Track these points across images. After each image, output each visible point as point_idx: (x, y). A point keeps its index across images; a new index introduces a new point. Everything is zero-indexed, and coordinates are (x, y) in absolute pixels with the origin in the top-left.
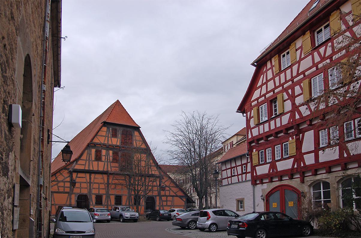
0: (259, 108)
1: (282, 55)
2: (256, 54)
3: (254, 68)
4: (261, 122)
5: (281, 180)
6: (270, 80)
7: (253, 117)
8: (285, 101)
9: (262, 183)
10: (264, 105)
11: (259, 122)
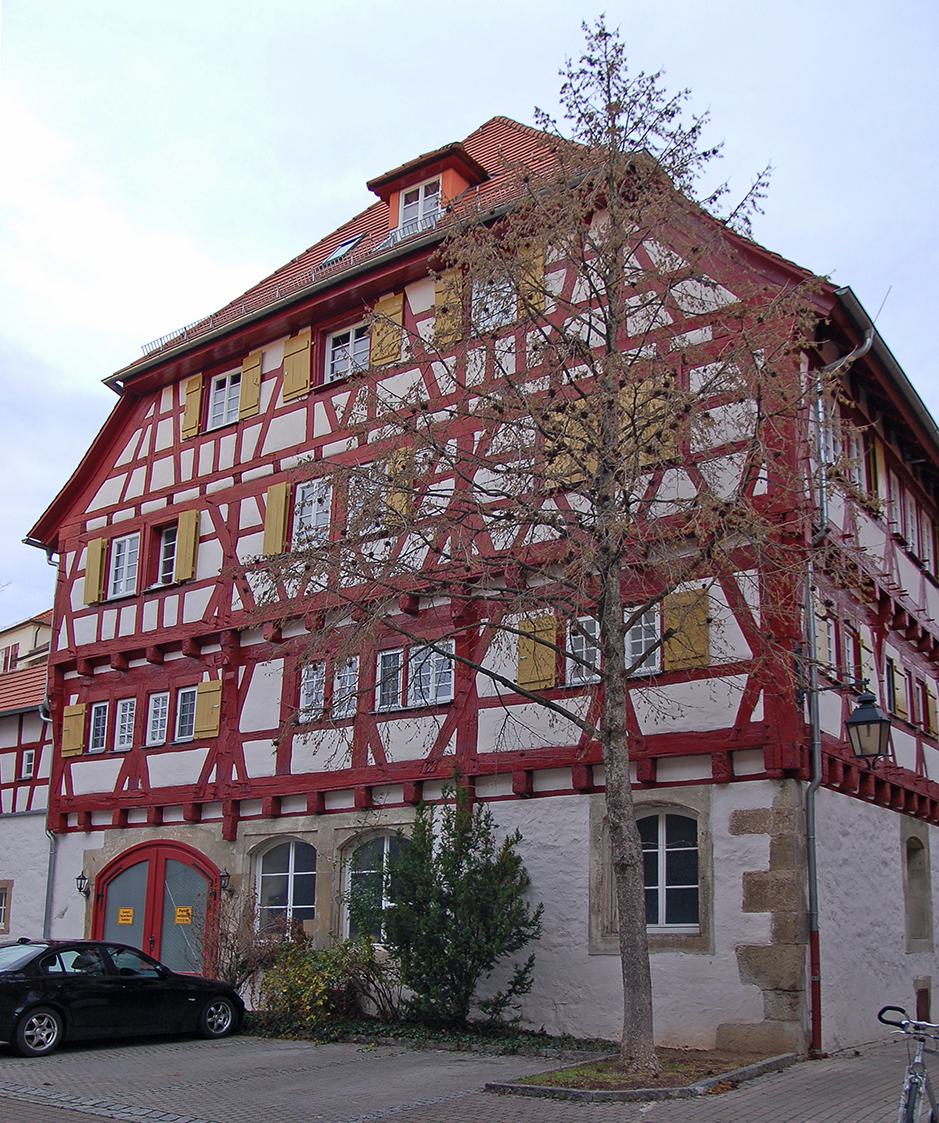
0: (110, 543)
1: (215, 380)
2: (128, 354)
3: (114, 398)
4: (111, 596)
6: (165, 454)
7: (83, 573)
8: (203, 539)
10: (131, 540)
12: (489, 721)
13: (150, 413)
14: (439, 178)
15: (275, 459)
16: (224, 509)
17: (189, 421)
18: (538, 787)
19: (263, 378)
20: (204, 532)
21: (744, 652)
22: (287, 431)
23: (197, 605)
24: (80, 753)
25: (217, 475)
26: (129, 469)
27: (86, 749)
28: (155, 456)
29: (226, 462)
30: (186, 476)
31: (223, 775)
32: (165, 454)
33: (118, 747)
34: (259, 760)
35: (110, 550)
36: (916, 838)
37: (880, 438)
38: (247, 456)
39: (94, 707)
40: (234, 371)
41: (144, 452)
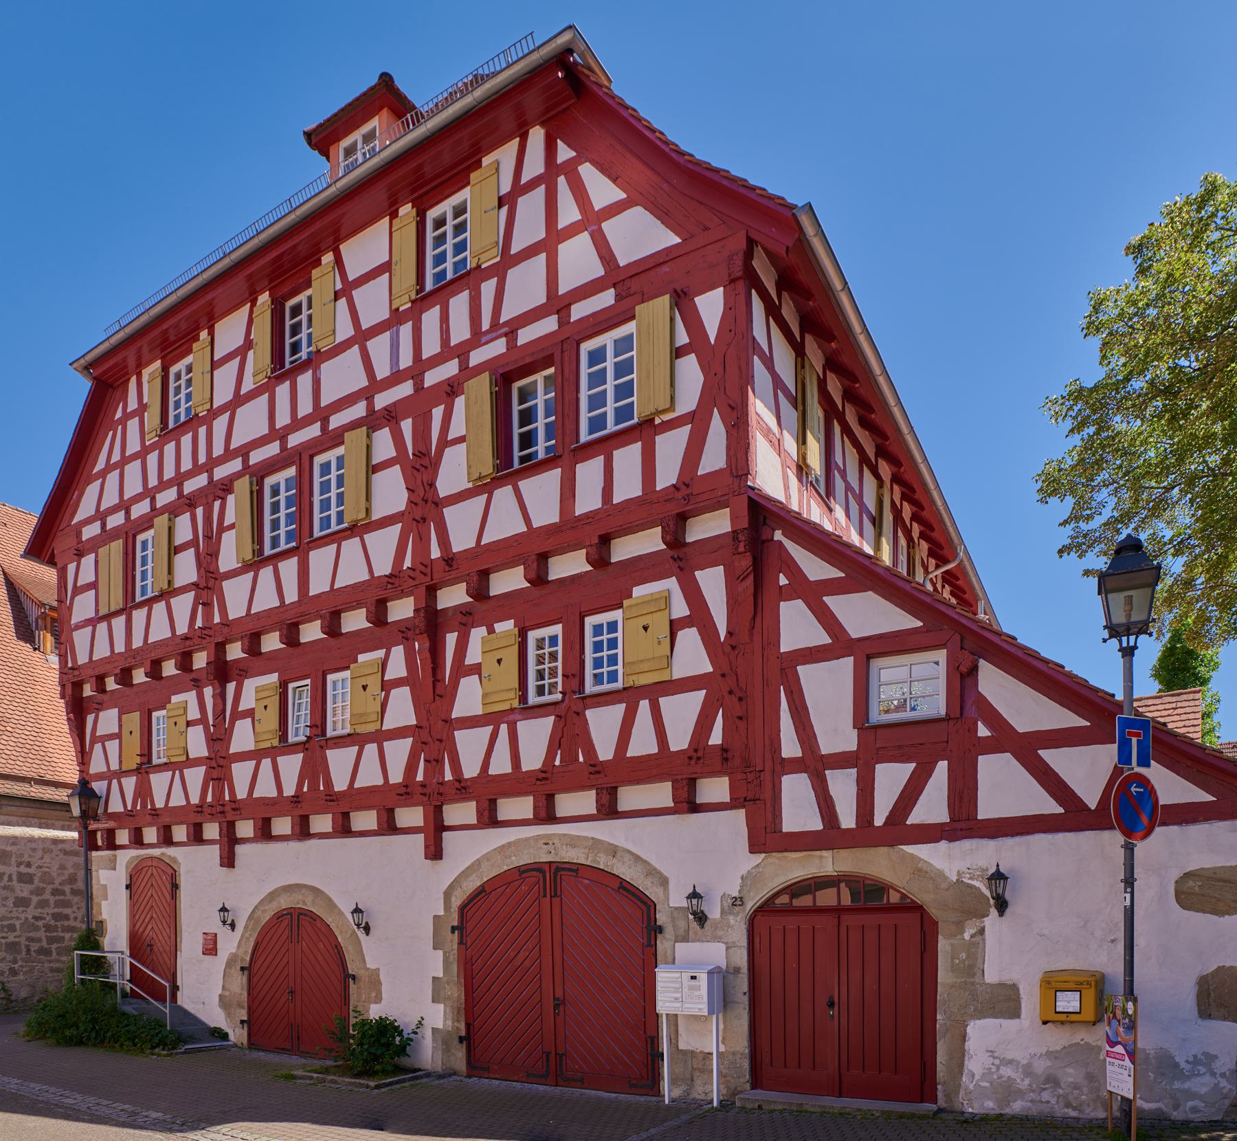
0: (260, 483)
1: (432, 214)
2: (99, 329)
3: (83, 386)
4: (268, 551)
5: (545, 815)
6: (134, 457)
7: (232, 526)
9: (489, 819)
11: (261, 551)
12: (241, 773)
13: (119, 415)
14: (374, 123)
15: (244, 451)
16: (407, 426)
17: (152, 418)
18: (701, 799)
19: (214, 365)
20: (377, 459)
21: (705, 666)
22: (251, 422)
23: (383, 548)
24: (276, 742)
25: (297, 424)
26: (103, 474)
27: (523, 698)
28: (125, 460)
29: (305, 407)
30: (382, 372)
31: (219, 794)
32: (134, 457)
33: (292, 739)
34: (470, 748)
35: (260, 493)
36: (1188, 875)
37: (767, 433)
38: (218, 450)
39: (590, 621)
40: (455, 199)
41: (116, 457)
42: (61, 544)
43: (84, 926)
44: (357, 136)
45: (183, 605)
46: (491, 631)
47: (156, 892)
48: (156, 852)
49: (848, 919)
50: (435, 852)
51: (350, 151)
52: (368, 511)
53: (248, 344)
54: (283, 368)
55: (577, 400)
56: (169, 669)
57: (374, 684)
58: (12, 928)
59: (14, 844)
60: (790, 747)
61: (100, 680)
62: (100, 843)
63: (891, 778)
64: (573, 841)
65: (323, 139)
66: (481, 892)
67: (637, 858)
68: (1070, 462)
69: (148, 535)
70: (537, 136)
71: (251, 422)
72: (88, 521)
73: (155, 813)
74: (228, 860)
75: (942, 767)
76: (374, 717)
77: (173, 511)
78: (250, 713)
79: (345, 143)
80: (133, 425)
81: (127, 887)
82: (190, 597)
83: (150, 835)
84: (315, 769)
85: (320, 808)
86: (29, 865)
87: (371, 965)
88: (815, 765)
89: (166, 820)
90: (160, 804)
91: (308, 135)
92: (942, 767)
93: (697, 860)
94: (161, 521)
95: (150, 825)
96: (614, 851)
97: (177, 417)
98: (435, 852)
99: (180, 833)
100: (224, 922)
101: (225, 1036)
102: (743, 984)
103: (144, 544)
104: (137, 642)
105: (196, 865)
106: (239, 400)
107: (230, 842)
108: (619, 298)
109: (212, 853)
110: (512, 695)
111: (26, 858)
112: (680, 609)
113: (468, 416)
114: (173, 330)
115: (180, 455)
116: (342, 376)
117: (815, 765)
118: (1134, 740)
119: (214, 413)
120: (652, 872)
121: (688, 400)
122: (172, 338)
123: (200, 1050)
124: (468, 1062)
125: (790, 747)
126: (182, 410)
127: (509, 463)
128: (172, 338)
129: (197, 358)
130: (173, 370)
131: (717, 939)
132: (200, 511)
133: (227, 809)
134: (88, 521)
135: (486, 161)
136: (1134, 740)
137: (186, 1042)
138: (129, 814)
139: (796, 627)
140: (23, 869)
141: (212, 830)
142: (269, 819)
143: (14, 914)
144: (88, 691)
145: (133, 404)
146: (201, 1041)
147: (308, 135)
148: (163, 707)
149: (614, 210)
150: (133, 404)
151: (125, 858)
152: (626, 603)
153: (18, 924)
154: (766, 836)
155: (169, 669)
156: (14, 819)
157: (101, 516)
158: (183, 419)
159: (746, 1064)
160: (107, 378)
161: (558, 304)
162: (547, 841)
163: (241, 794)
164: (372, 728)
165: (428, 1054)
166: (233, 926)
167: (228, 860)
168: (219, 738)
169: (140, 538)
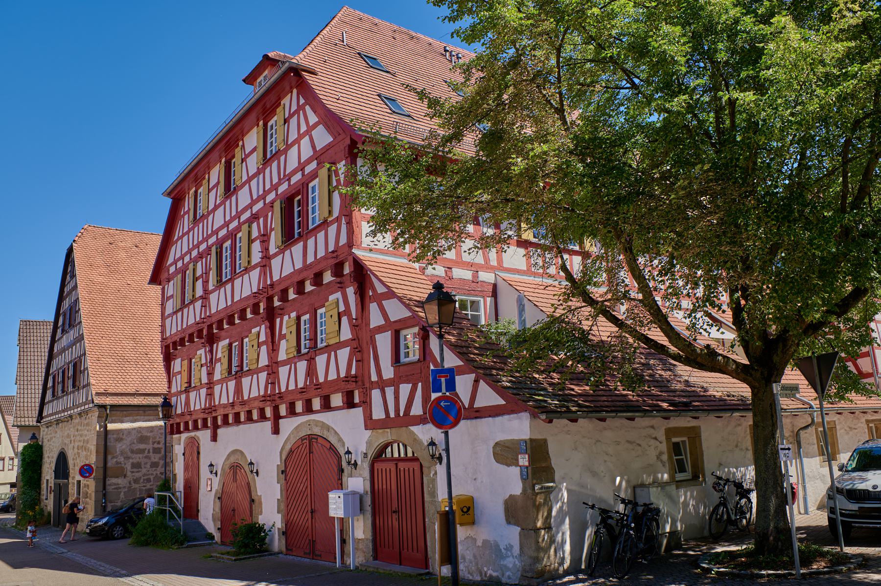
2: (170, 178)
3: (169, 201)
11: (221, 280)
14: (266, 72)
19: (209, 191)
22: (218, 219)
42: (164, 276)
43: (163, 477)
44: (261, 78)
45: (255, 274)
46: (290, 317)
47: (193, 451)
48: (193, 434)
49: (401, 465)
50: (276, 431)
51: (260, 82)
52: (249, 262)
53: (218, 183)
54: (230, 190)
55: (308, 210)
56: (328, 277)
57: (255, 343)
58: (149, 480)
59: (152, 432)
60: (374, 378)
61: (285, 292)
62: (230, 421)
63: (405, 389)
64: (316, 422)
65: (250, 80)
66: (291, 452)
67: (336, 432)
68: (451, 234)
69: (315, 182)
70: (295, 91)
71: (218, 219)
72: (171, 265)
73: (318, 386)
74: (214, 438)
75: (420, 384)
76: (254, 361)
77: (194, 261)
78: (220, 359)
79: (258, 81)
80: (186, 217)
81: (184, 454)
82: (258, 270)
83: (316, 404)
84: (311, 371)
85: (314, 396)
86: (159, 443)
87: (259, 494)
88: (382, 385)
89: (325, 392)
90: (192, 409)
91: (244, 81)
92: (420, 384)
93: (349, 431)
94: (245, 227)
95: (316, 396)
96: (328, 428)
97: (271, 151)
98: (276, 431)
99: (337, 400)
100: (211, 472)
101: (212, 537)
102: (368, 500)
103: (313, 188)
104: (310, 259)
105: (204, 436)
106: (216, 207)
107: (277, 417)
108: (318, 164)
109: (268, 425)
110: (293, 350)
111: (158, 439)
112: (342, 308)
113: (275, 220)
114: (195, 174)
115: (198, 234)
116: (243, 198)
117: (382, 385)
118: (443, 379)
119: (209, 213)
120: (340, 440)
121: (336, 213)
122: (268, 106)
123: (200, 545)
124: (286, 548)
125: (374, 378)
126: (273, 147)
127: (289, 238)
128: (268, 106)
129: (276, 120)
130: (270, 124)
131: (360, 476)
132: (261, 220)
133: (276, 398)
134: (171, 265)
135: (282, 103)
136: (443, 379)
137: (189, 541)
138: (302, 391)
139: (375, 319)
140: (156, 446)
141: (269, 412)
142: (310, 400)
143: (150, 472)
144: (277, 303)
145: (186, 209)
146: (199, 541)
147: (244, 81)
148: (323, 306)
149: (316, 125)
150: (186, 209)
151: (184, 436)
152: (326, 304)
153: (152, 477)
154: (370, 423)
155: (328, 277)
156: (152, 417)
157: (175, 262)
158: (274, 152)
159: (370, 545)
160: (177, 196)
161: (301, 167)
162: (308, 423)
163: (283, 390)
164: (254, 366)
165: (277, 543)
166: (216, 474)
167: (214, 438)
168: (210, 374)
169: (311, 185)
